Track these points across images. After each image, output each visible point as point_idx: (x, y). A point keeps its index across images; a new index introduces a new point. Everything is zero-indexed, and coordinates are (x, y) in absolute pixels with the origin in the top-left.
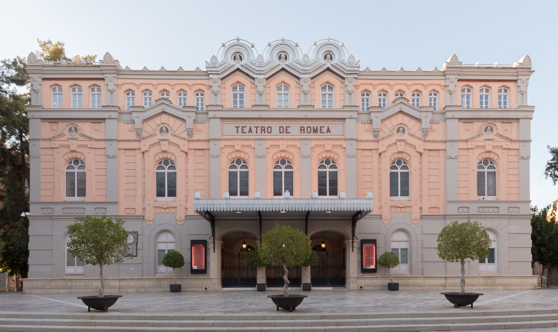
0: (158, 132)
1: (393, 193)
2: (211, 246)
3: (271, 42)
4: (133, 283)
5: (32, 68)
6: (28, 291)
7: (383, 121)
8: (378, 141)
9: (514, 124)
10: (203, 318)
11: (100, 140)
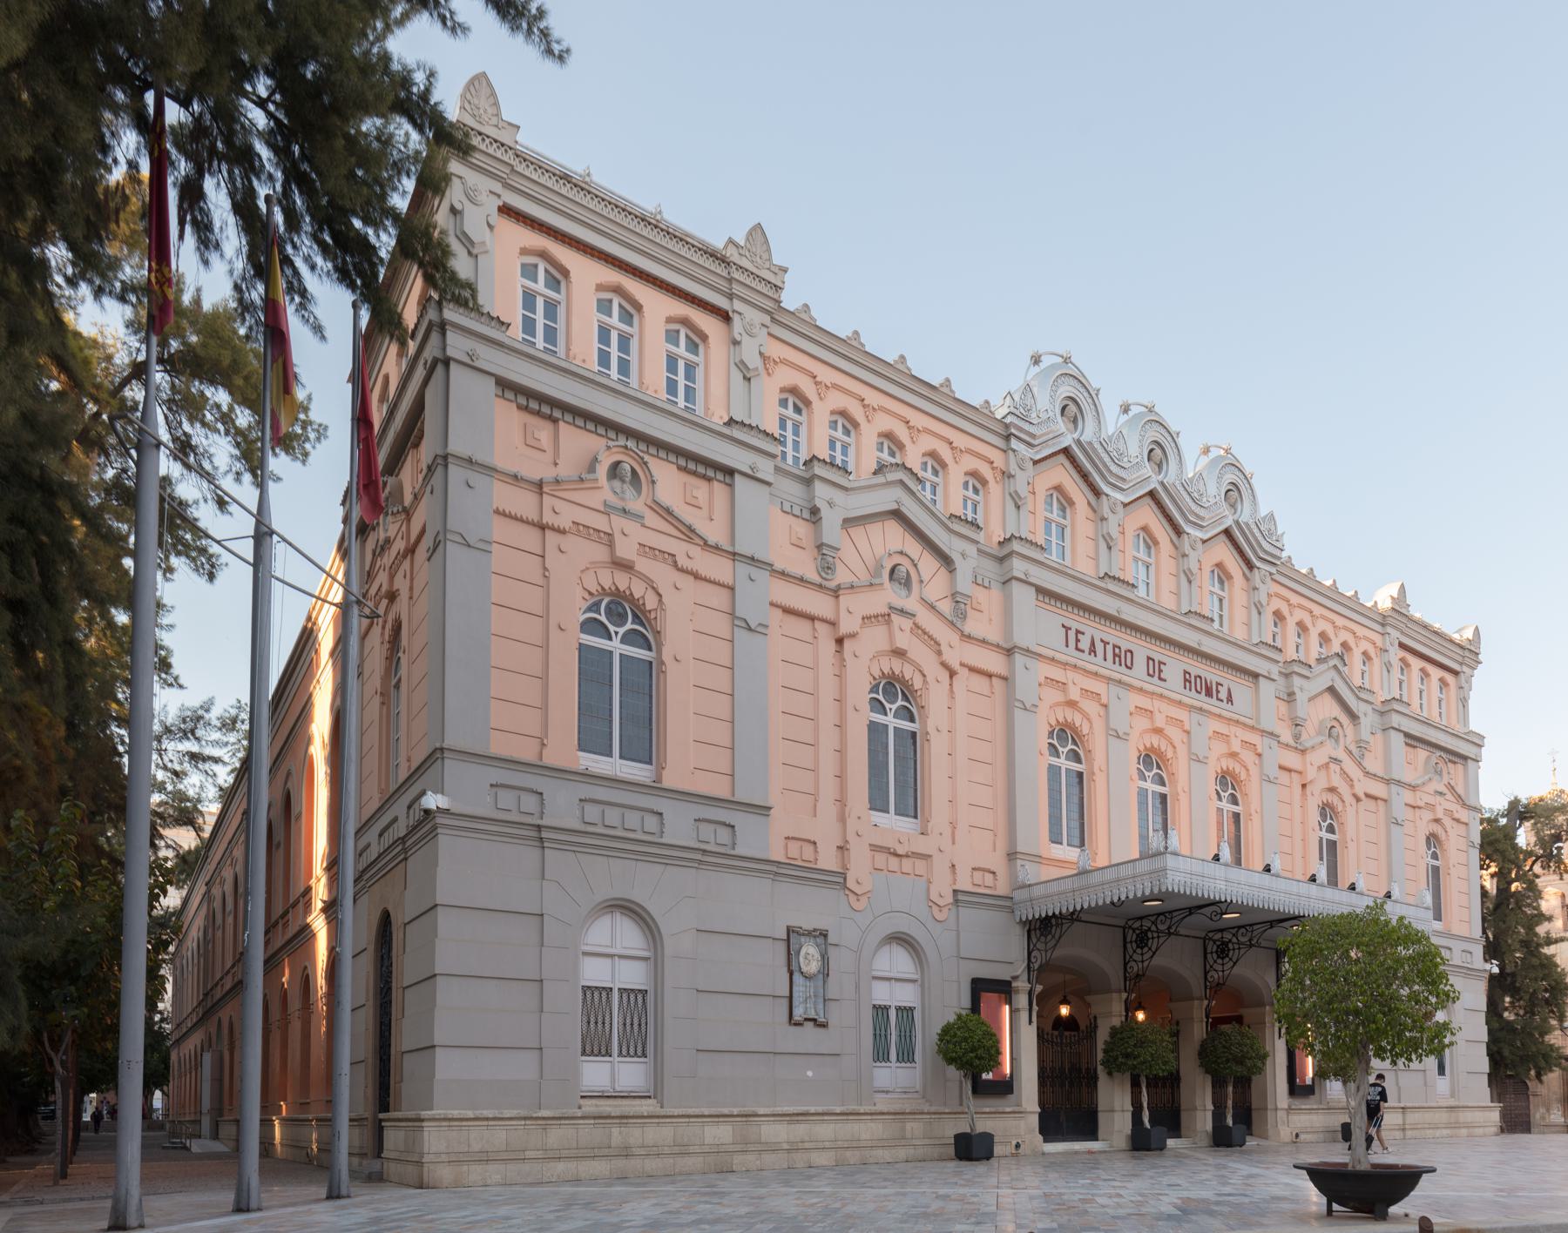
4: (825, 1131)
6: (445, 1173)
7: (848, 522)
8: (836, 593)
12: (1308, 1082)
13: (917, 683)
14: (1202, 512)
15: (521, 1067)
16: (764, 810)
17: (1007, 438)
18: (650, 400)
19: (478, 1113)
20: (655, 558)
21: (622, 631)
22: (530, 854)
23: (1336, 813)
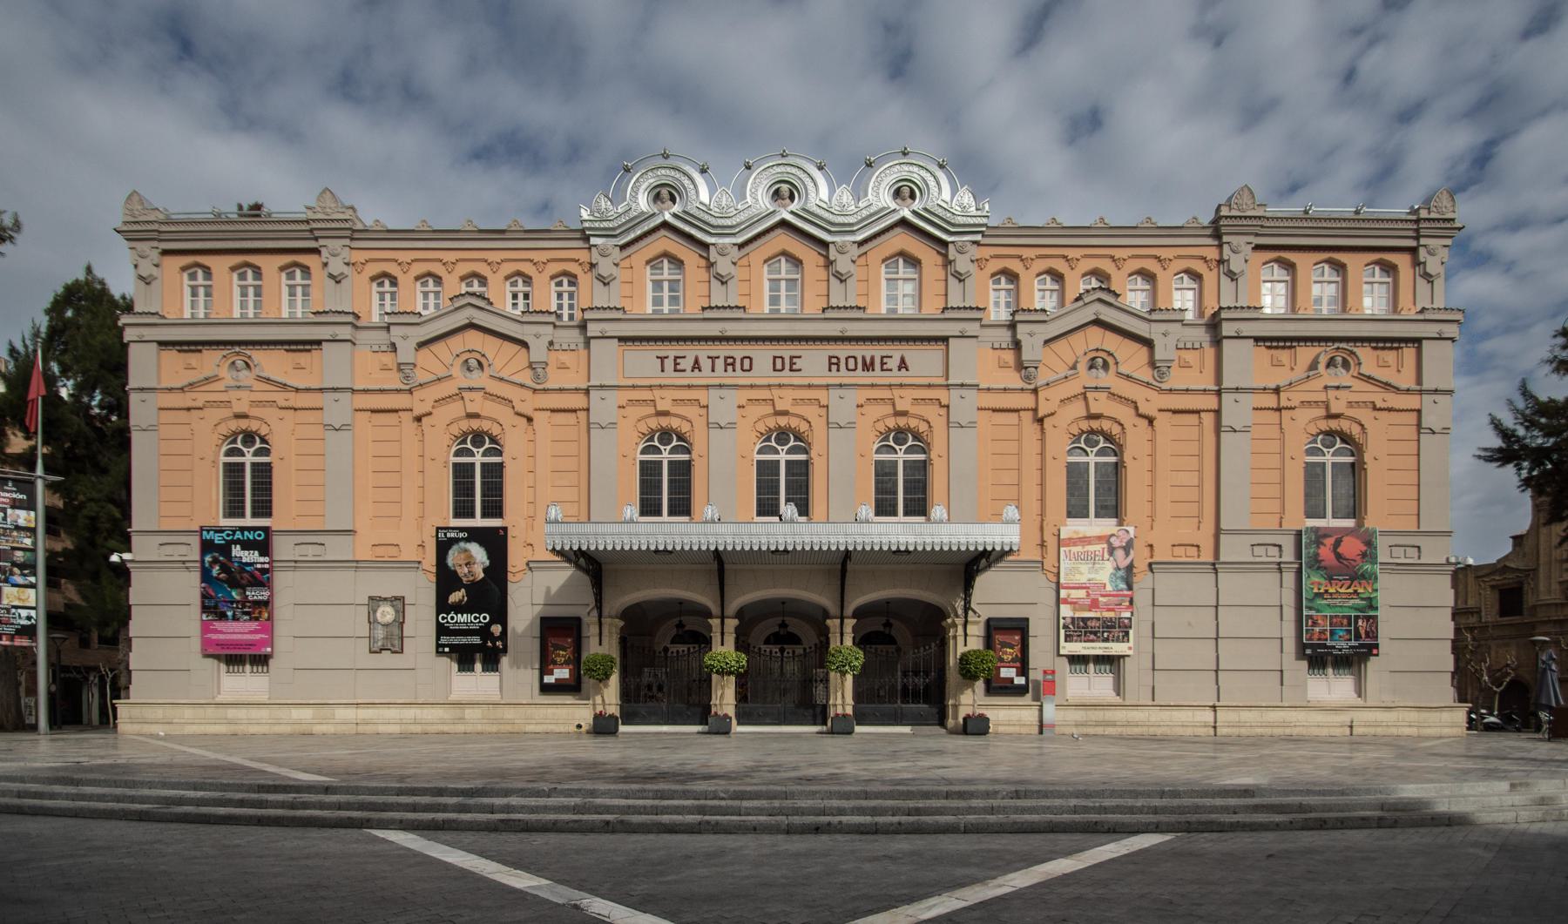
0: (1082, 367)
8: (410, 391)
17: (587, 239)
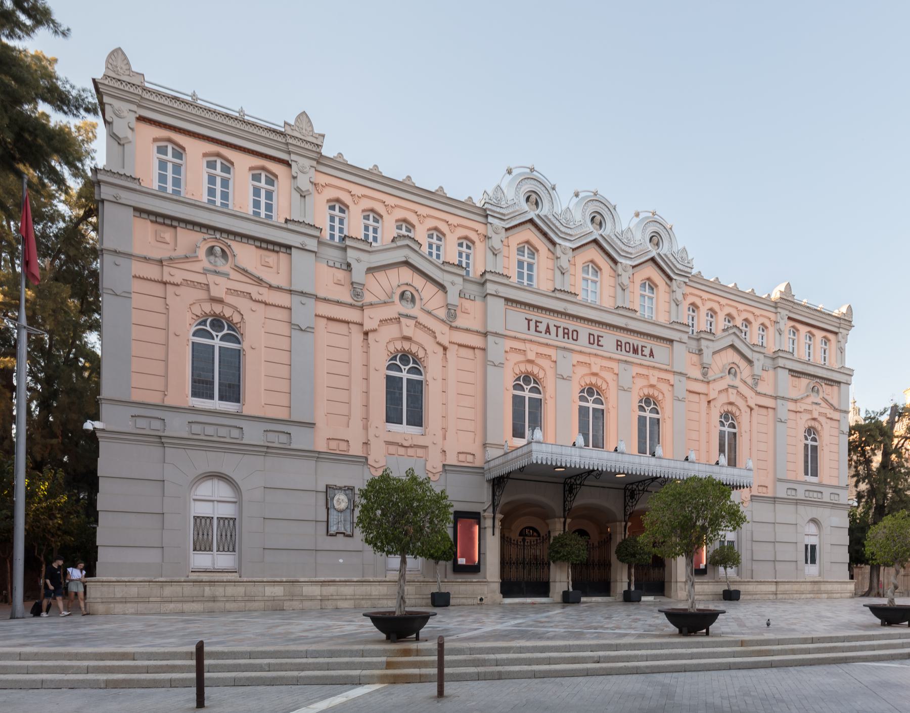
0: (396, 298)
1: (393, 417)
2: (488, 523)
3: (512, 167)
4: (347, 590)
5: (117, 85)
6: (100, 608)
7: (370, 270)
8: (362, 308)
9: (835, 388)
10: (617, 647)
11: (278, 288)
12: (702, 566)
13: (421, 354)
14: (630, 250)
15: (153, 557)
16: (312, 425)
17: (486, 216)
18: (233, 212)
19: (119, 579)
20: (238, 295)
21: (407, 368)
22: (771, 506)
23: (817, 432)
